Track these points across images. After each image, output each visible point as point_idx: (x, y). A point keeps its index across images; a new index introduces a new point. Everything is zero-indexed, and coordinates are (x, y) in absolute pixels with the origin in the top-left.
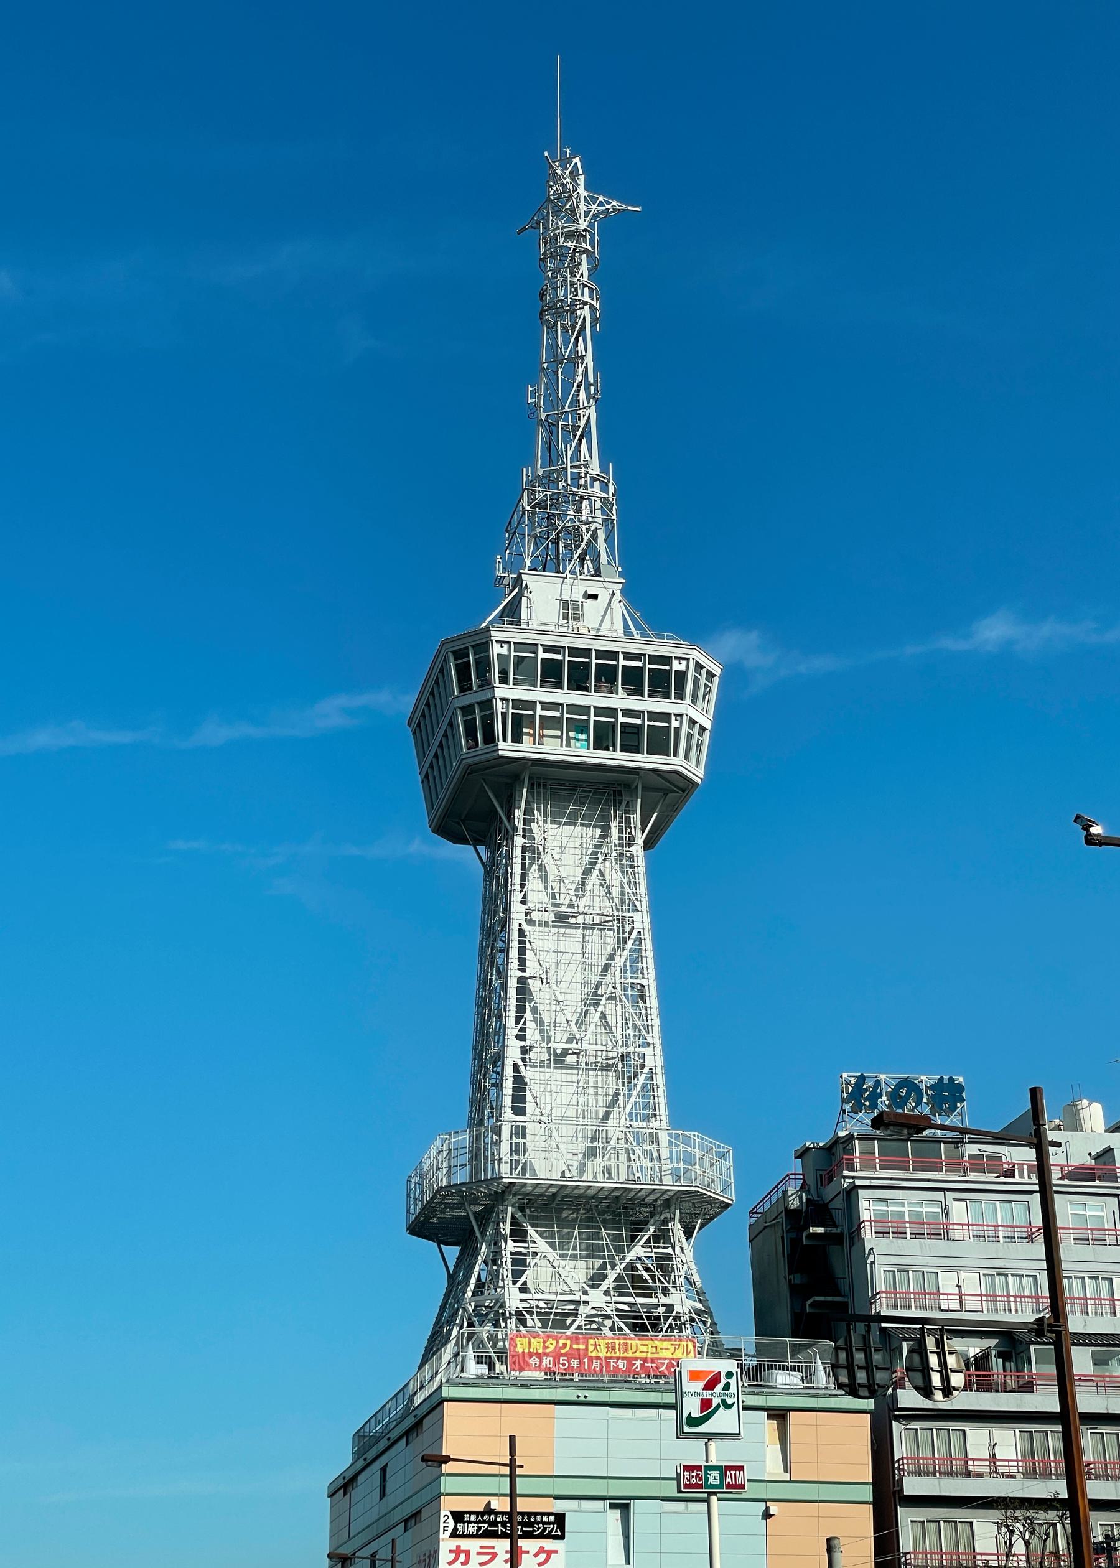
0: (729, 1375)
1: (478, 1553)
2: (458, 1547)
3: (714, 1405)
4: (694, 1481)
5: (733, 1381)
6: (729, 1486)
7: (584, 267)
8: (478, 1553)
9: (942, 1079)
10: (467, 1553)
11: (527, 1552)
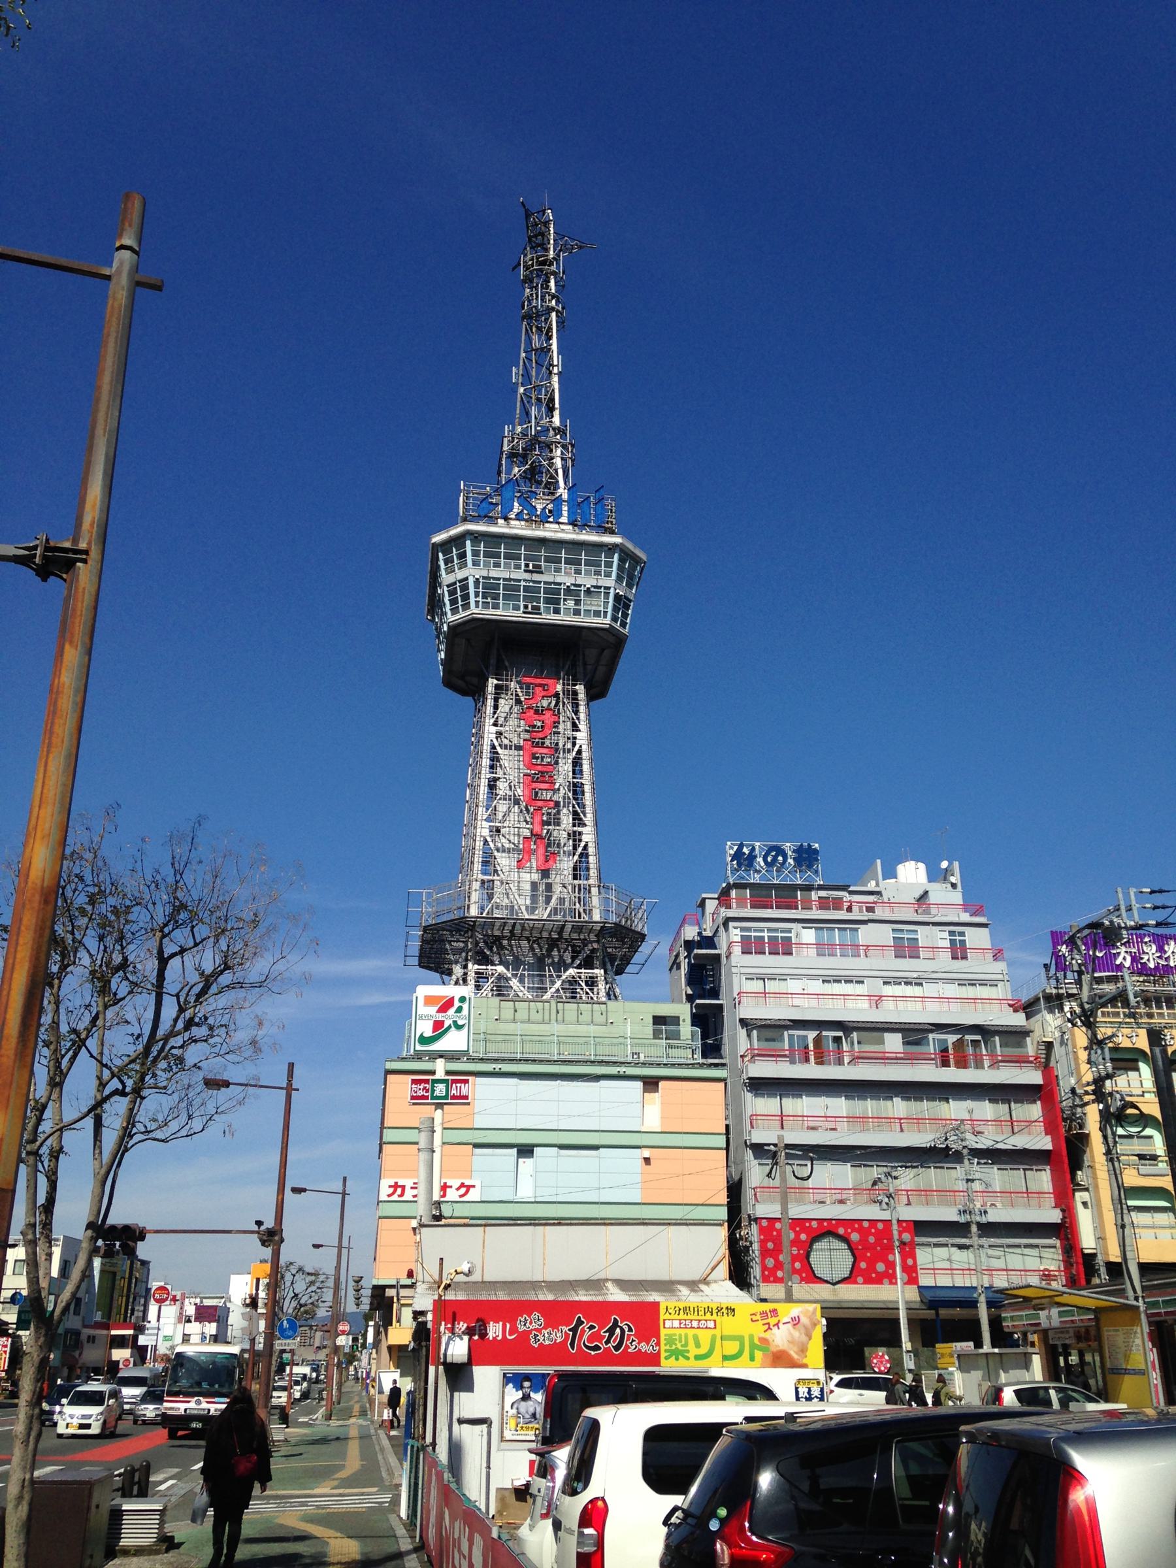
0: (463, 999)
1: (412, 1188)
2: (396, 1183)
3: (446, 1025)
4: (420, 1093)
5: (465, 1006)
6: (454, 1097)
7: (552, 284)
8: (412, 1188)
9: (802, 845)
10: (403, 1187)
11: (451, 1187)
